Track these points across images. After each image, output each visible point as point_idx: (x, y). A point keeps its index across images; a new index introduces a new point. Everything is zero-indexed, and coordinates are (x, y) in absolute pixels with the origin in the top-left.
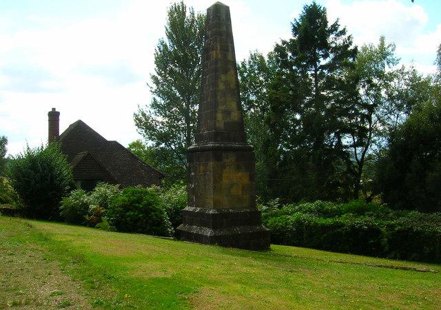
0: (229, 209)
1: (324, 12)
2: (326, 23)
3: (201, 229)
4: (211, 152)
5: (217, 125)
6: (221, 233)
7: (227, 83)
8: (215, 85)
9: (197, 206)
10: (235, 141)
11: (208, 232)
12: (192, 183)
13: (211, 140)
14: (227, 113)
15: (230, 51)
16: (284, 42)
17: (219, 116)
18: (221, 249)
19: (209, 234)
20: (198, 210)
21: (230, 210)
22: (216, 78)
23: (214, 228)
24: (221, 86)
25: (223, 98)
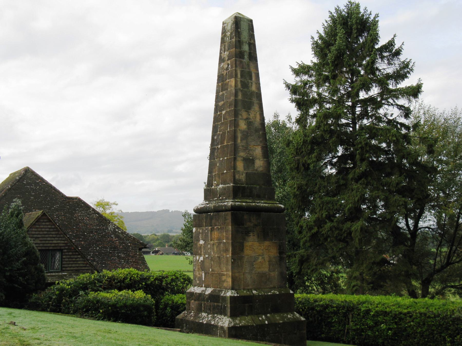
0: (251, 290)
1: (375, 23)
2: (375, 39)
3: (214, 318)
4: (229, 213)
5: (237, 177)
6: (243, 323)
7: (249, 123)
8: (235, 124)
9: (206, 287)
10: (259, 197)
11: (225, 322)
12: (200, 255)
13: (228, 197)
14: (249, 161)
15: (254, 79)
16: (301, 70)
17: (240, 165)
18: (136, 325)
19: (226, 325)
20: (209, 291)
21: (254, 292)
22: (236, 114)
23: (233, 315)
24: (243, 125)
25: (245, 141)
